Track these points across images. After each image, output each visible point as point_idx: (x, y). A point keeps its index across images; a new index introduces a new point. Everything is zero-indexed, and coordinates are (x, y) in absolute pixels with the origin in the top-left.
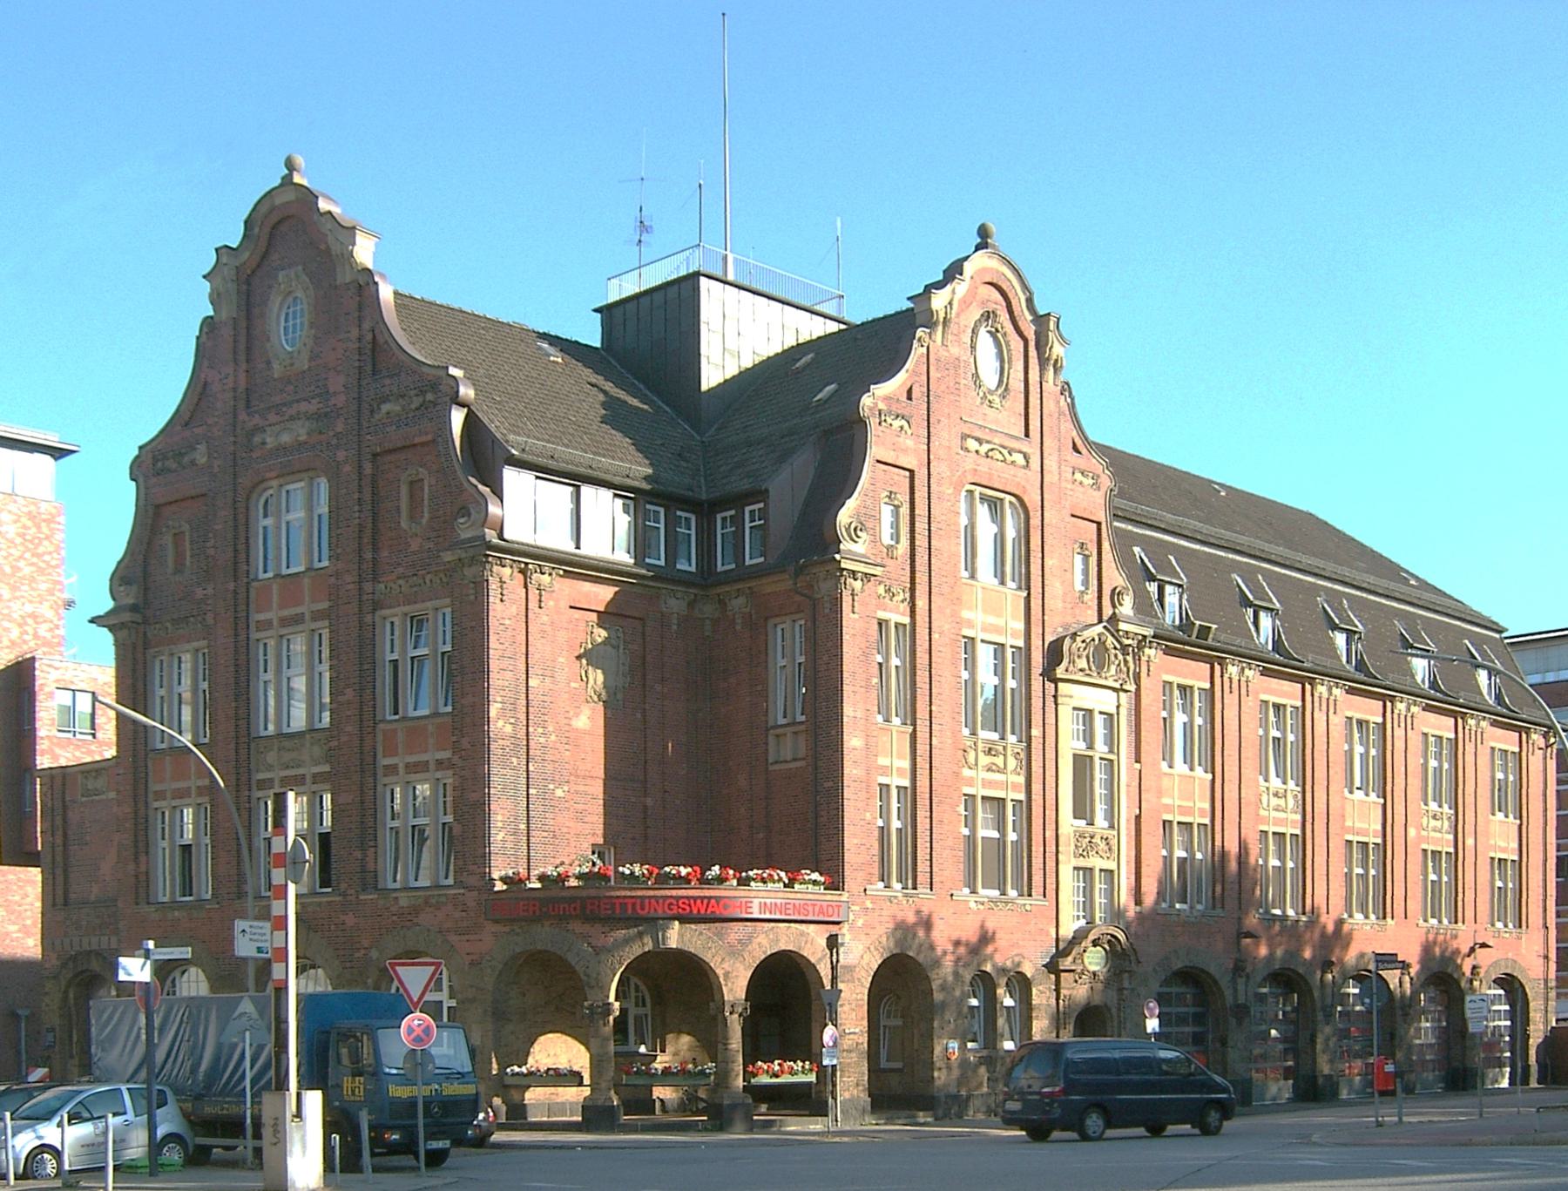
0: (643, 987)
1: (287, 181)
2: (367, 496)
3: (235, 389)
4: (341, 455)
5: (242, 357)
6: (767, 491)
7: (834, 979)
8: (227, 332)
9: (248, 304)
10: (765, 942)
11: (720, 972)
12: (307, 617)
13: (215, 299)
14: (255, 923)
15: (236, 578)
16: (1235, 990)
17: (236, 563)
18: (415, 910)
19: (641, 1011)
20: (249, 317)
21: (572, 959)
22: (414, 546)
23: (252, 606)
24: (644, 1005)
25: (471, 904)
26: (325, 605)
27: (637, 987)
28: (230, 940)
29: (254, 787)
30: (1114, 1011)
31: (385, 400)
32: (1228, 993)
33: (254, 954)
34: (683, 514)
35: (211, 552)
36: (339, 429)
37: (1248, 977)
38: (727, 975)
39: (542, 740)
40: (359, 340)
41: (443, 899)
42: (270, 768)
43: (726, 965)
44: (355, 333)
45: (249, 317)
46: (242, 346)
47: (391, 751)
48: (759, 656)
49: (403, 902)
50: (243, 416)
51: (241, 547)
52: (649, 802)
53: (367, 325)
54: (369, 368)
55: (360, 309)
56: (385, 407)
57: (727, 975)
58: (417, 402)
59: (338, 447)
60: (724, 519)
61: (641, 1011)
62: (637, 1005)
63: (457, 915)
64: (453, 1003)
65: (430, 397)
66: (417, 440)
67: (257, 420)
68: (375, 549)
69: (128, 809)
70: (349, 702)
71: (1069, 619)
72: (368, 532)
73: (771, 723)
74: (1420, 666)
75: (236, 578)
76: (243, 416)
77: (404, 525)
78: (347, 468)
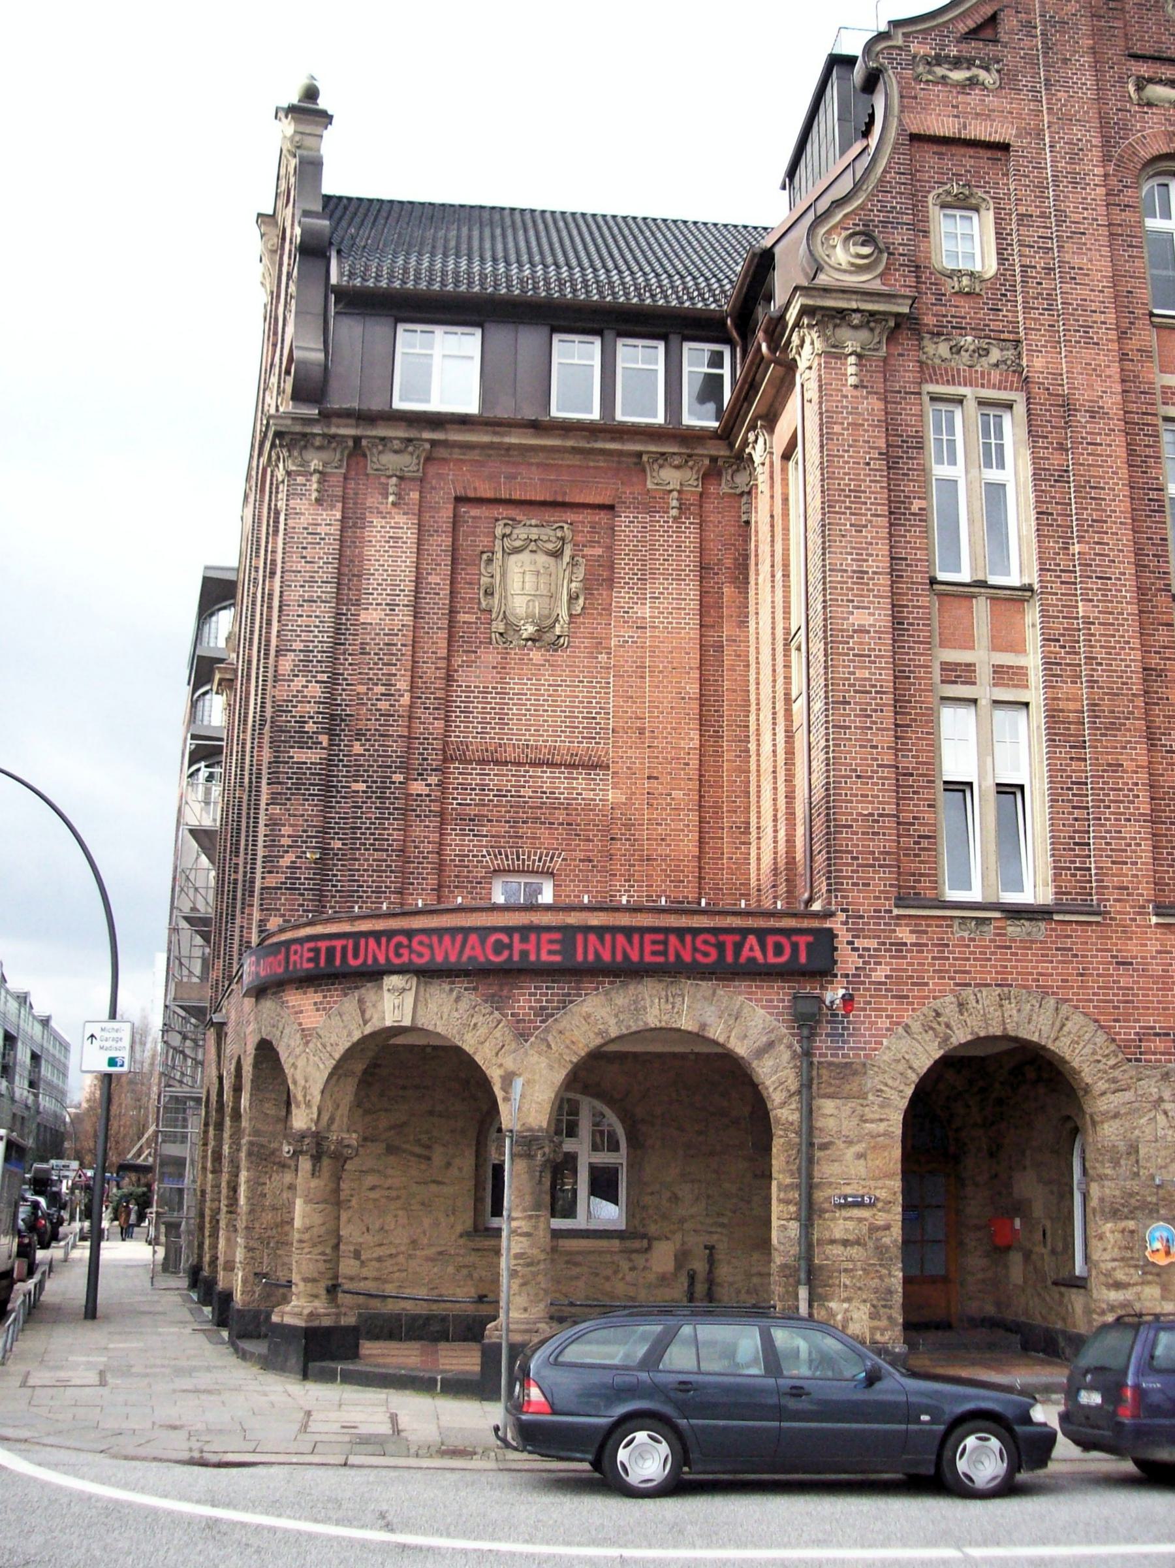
7: (807, 1091)
11: (495, 1075)
61: (604, 1158)
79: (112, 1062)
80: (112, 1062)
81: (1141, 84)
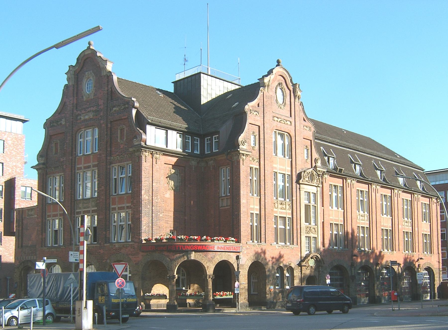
0: (184, 270)
1: (89, 48)
2: (109, 133)
3: (73, 104)
4: (102, 122)
5: (75, 95)
6: (219, 132)
7: (238, 268)
8: (71, 89)
9: (77, 81)
10: (218, 258)
11: (206, 266)
12: (91, 166)
13: (68, 80)
14: (75, 252)
15: (72, 156)
16: (351, 271)
17: (72, 151)
18: (120, 249)
19: (183, 277)
20: (77, 84)
21: (164, 262)
22: (122, 147)
23: (76, 163)
24: (184, 276)
25: (136, 247)
26: (97, 163)
27: (182, 271)
28: (68, 257)
29: (76, 214)
30: (317, 277)
31: (114, 107)
32: (349, 272)
33: (74, 261)
34: (196, 138)
35: (65, 148)
36: (101, 115)
37: (355, 267)
38: (208, 267)
39: (156, 201)
40: (108, 90)
41: (128, 245)
42: (80, 208)
43: (208, 264)
44: (106, 89)
45: (77, 84)
46: (75, 92)
47: (114, 204)
48: (217, 177)
49: (117, 246)
50: (75, 111)
51: (74, 147)
52: (186, 218)
53: (110, 87)
54: (110, 98)
55: (108, 82)
56: (114, 109)
57: (208, 267)
58: (123, 107)
59: (101, 119)
60: (207, 139)
61: (183, 277)
62: (182, 276)
63: (132, 250)
64: (130, 275)
65: (126, 106)
66: (123, 118)
67: (79, 112)
68: (111, 147)
69: (40, 220)
70: (103, 190)
71: (303, 167)
72: (109, 143)
73: (220, 196)
74: (401, 180)
75: (72, 156)
76: (75, 111)
77: (119, 141)
78: (104, 125)
79: (76, 260)
80: (76, 260)
81: (274, 117)
